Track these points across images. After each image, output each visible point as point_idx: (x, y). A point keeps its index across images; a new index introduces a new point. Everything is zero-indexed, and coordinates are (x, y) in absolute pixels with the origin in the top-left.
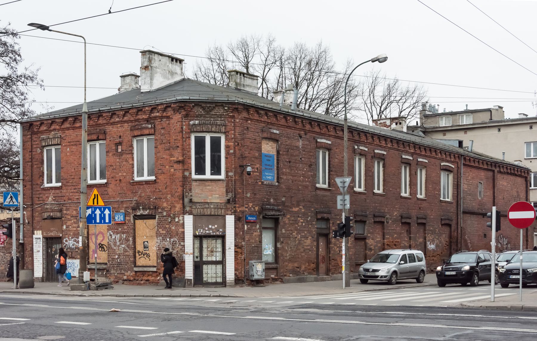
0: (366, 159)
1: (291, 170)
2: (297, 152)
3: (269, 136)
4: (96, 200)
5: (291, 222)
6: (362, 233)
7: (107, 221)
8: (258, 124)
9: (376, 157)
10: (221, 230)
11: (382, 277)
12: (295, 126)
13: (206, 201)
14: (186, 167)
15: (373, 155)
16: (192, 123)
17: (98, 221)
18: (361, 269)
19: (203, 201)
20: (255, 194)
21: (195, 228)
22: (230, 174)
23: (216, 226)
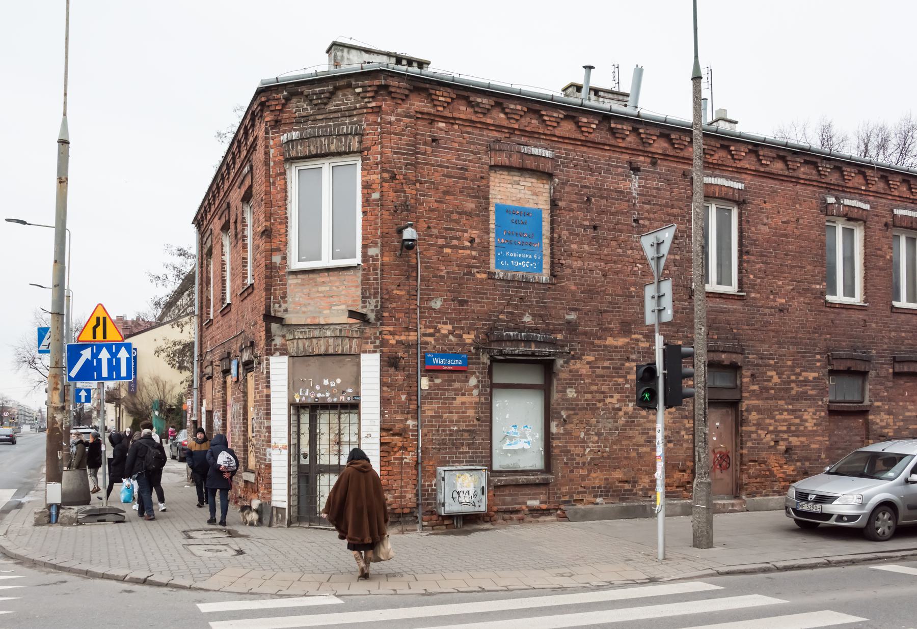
0: (866, 228)
1: (600, 246)
2: (624, 206)
3: (515, 161)
4: (100, 330)
5: (599, 371)
6: (857, 398)
7: (124, 373)
8: (477, 132)
9: (897, 224)
10: (349, 390)
11: (840, 518)
12: (613, 142)
13: (317, 321)
14: (274, 245)
15: (889, 220)
16: (284, 138)
17: (105, 374)
18: (792, 492)
19: (309, 321)
20: (463, 303)
21: (293, 385)
22: (373, 251)
23: (339, 381)
